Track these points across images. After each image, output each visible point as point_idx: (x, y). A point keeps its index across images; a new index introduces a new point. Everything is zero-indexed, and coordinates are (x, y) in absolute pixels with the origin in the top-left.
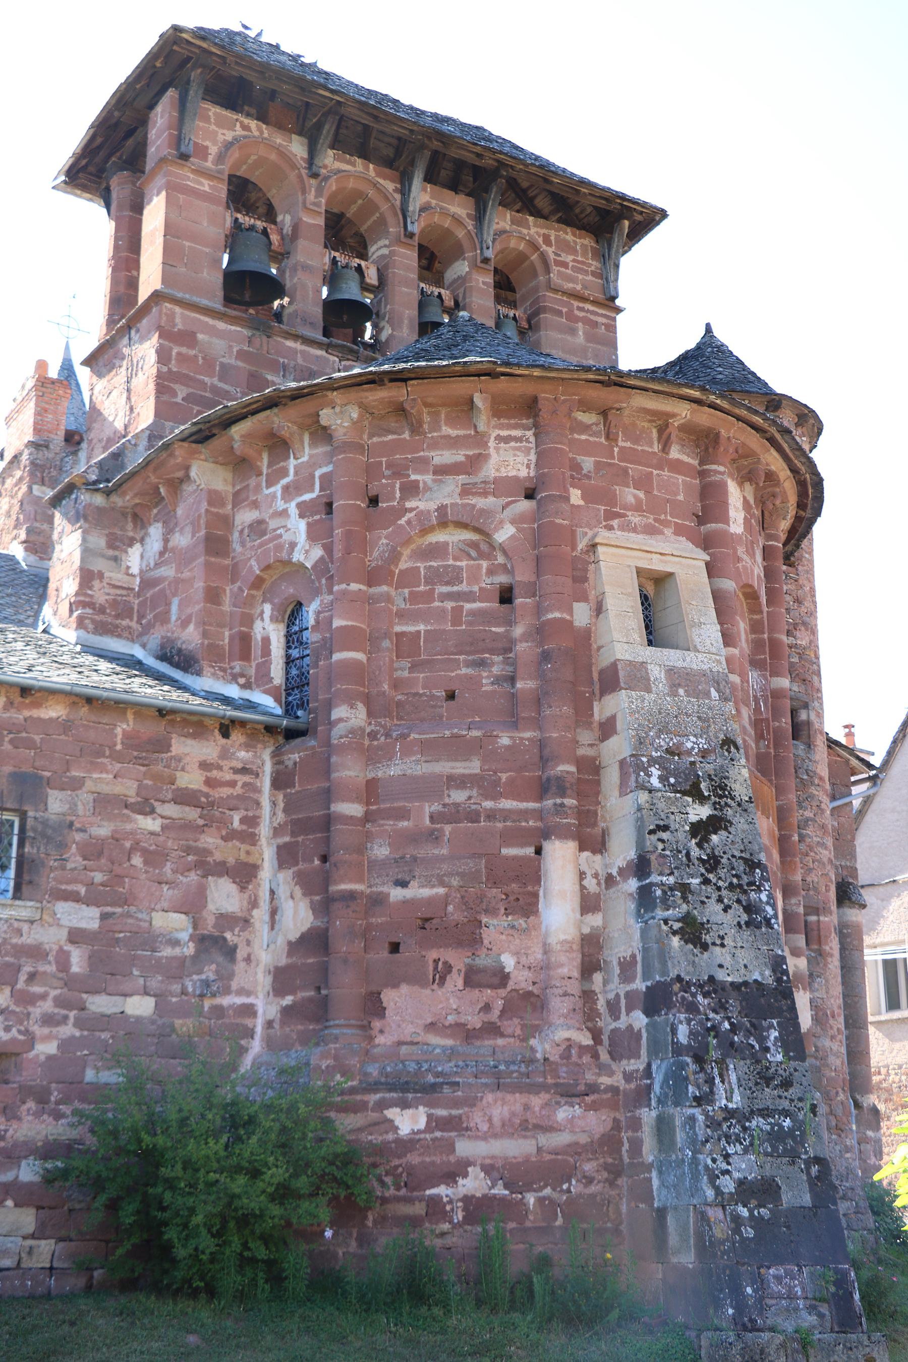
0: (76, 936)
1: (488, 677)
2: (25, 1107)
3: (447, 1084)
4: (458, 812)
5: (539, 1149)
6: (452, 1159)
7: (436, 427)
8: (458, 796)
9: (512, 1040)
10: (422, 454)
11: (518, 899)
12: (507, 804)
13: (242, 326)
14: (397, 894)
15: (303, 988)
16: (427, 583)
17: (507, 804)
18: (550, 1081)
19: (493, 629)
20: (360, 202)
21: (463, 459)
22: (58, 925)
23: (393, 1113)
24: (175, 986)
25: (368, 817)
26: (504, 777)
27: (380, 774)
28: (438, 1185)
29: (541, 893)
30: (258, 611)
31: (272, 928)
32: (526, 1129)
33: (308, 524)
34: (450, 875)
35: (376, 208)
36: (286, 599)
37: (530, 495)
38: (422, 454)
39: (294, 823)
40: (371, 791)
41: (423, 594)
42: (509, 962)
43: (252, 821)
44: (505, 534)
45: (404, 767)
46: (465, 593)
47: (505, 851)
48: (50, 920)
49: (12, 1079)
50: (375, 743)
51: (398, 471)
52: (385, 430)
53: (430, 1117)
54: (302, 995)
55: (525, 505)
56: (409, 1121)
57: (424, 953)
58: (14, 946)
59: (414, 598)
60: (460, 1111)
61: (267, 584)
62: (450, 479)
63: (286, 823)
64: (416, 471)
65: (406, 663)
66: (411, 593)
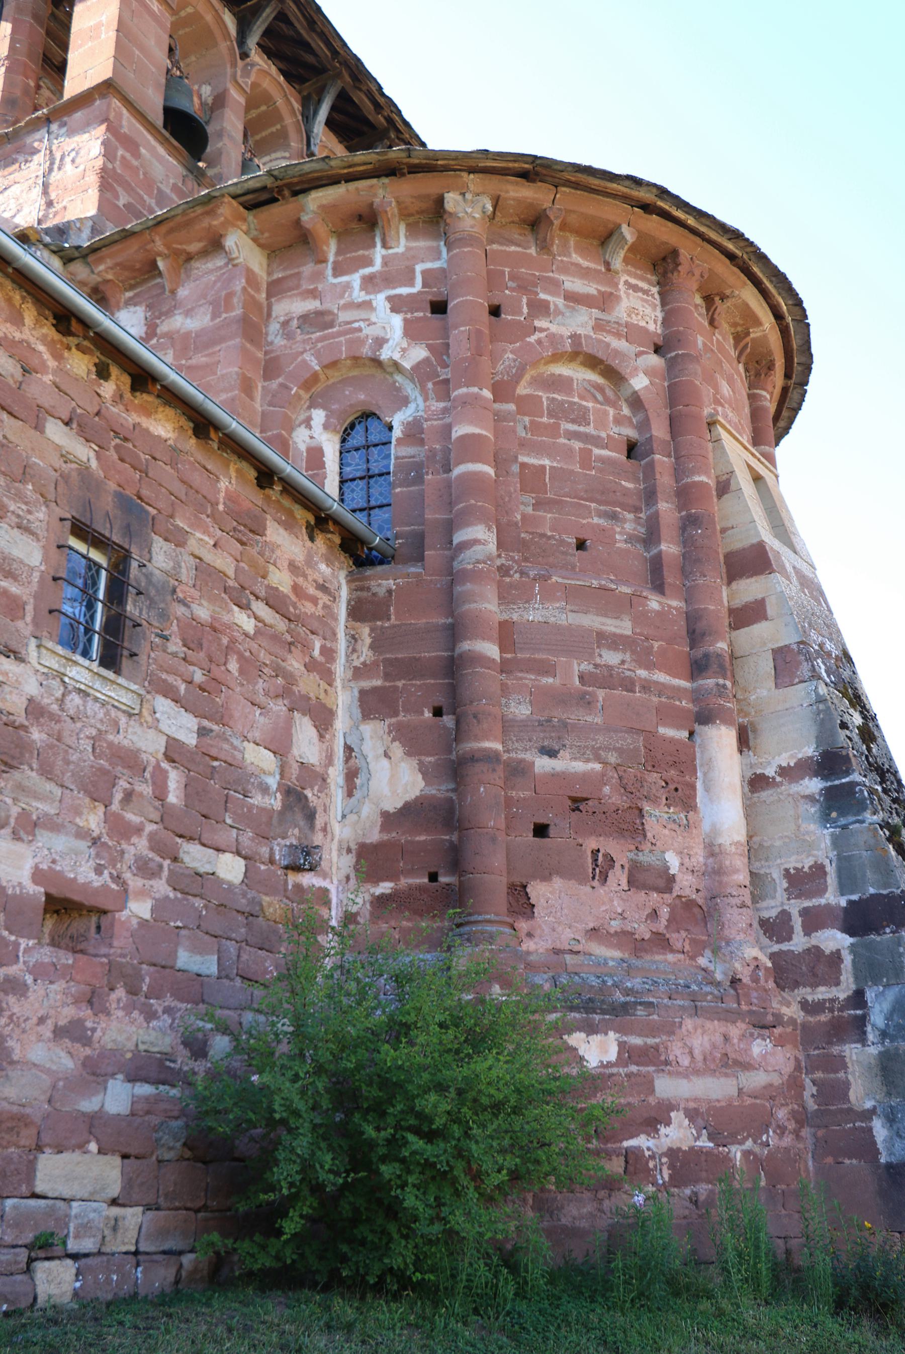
0: (174, 752)
1: (620, 533)
2: (113, 996)
3: (641, 1004)
4: (611, 675)
5: (740, 1090)
6: (652, 1100)
7: (565, 252)
8: (611, 658)
9: (681, 956)
10: (551, 274)
11: (676, 790)
12: (661, 677)
13: (179, 162)
14: (543, 764)
15: (409, 873)
16: (550, 415)
17: (661, 677)
18: (744, 1007)
19: (623, 483)
20: (264, 108)
21: (595, 292)
22: (156, 728)
23: (576, 1039)
24: (264, 849)
25: (505, 667)
26: (656, 645)
27: (515, 617)
28: (637, 1135)
29: (699, 785)
30: (302, 417)
31: (350, 794)
32: (726, 1065)
33: (406, 321)
34: (607, 749)
35: (280, 119)
36: (351, 406)
37: (657, 350)
38: (551, 274)
39: (388, 662)
40: (506, 634)
41: (546, 426)
42: (673, 862)
43: (329, 653)
44: (639, 383)
45: (544, 612)
46: (593, 436)
47: (662, 730)
48: (149, 719)
49: (92, 951)
50: (508, 580)
51: (525, 286)
52: (507, 240)
53: (622, 1045)
54: (405, 882)
55: (654, 360)
56: (597, 1050)
57: (580, 841)
58: (111, 745)
59: (535, 427)
60: (657, 1040)
61: (319, 387)
62: (583, 309)
63: (375, 663)
64: (545, 290)
65: (529, 499)
66: (532, 422)
